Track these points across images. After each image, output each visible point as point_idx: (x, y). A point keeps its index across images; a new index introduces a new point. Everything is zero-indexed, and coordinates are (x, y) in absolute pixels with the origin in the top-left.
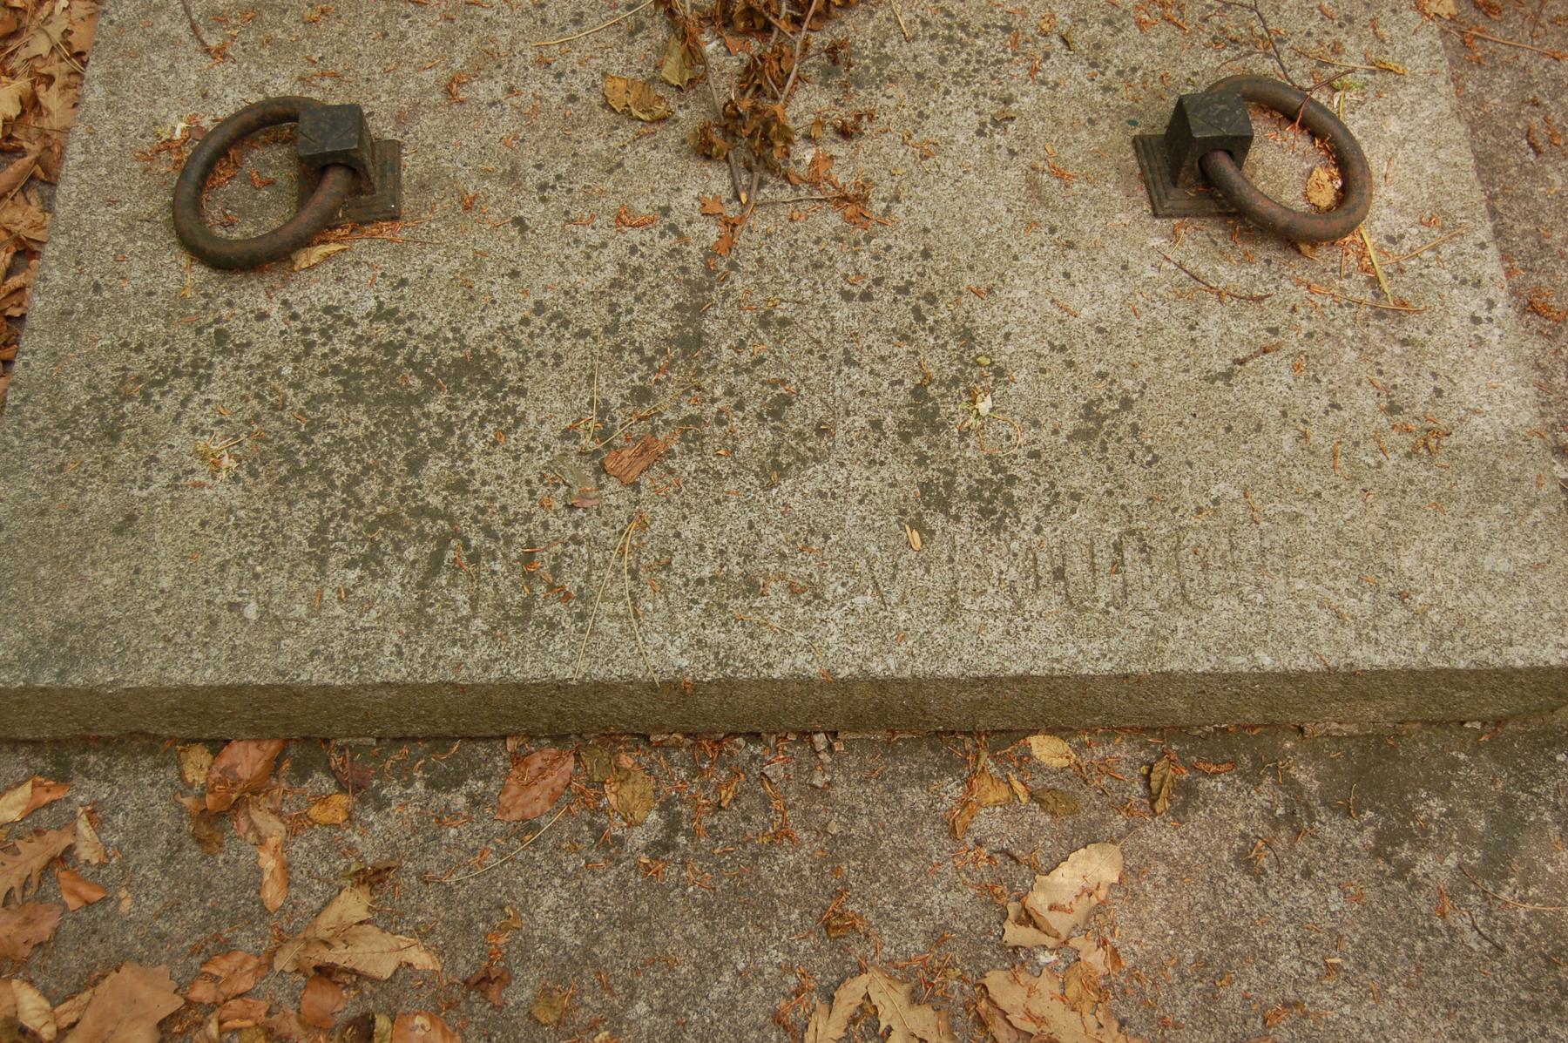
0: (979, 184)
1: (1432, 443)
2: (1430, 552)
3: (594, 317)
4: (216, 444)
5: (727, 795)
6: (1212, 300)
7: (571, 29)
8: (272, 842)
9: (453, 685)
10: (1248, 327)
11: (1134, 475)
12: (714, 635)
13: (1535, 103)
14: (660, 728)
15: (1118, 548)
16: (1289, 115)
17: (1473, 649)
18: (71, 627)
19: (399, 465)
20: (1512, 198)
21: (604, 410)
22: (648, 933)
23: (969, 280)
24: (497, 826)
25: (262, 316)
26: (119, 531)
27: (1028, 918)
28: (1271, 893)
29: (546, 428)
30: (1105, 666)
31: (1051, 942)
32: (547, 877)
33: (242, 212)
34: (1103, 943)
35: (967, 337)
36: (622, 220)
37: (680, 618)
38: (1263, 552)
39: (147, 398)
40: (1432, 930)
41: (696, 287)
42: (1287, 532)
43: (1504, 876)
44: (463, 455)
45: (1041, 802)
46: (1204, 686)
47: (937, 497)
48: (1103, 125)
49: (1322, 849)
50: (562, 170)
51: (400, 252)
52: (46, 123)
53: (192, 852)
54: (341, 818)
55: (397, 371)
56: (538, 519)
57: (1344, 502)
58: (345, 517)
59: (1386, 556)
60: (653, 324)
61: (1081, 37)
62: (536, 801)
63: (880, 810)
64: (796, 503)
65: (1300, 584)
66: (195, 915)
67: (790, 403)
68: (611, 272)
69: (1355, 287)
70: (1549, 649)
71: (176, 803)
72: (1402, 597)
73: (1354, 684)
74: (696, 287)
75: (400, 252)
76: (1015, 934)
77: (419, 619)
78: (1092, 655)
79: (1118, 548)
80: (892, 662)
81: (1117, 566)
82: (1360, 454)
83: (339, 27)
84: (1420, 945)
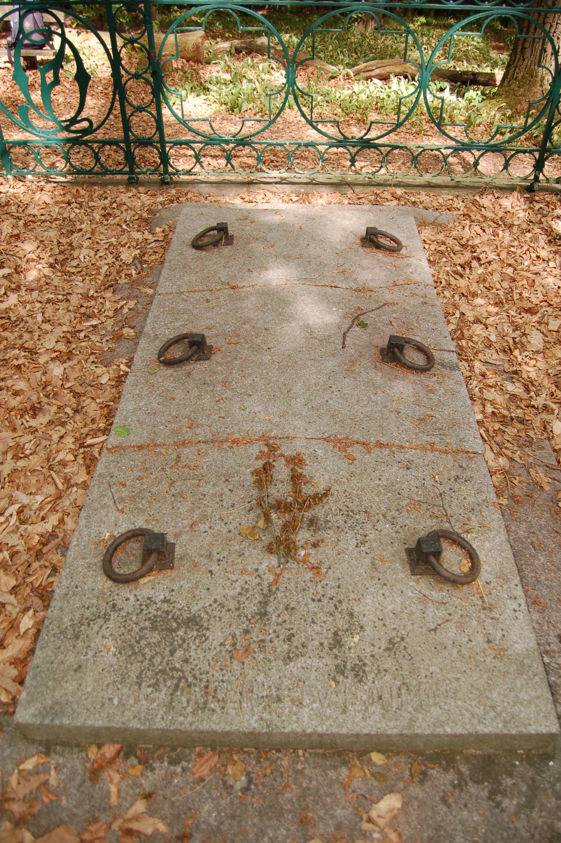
0: (356, 563)
1: (502, 653)
2: (502, 692)
3: (232, 605)
4: (110, 643)
5: (268, 771)
6: (430, 604)
7: (231, 509)
8: (116, 781)
9: (180, 730)
10: (441, 613)
11: (405, 663)
12: (266, 716)
13: (534, 533)
14: (247, 746)
15: (399, 689)
16: (454, 542)
17: (517, 727)
18: (57, 703)
19: (167, 652)
20: (528, 565)
21: (234, 637)
22: (239, 822)
23: (352, 596)
24: (191, 779)
25: (128, 599)
26: (76, 671)
27: (370, 820)
28: (454, 813)
29: (215, 642)
30: (395, 731)
31: (378, 829)
32: (207, 799)
33: (125, 564)
34: (395, 830)
35: (351, 615)
36: (244, 572)
37: (255, 710)
38: (447, 691)
39: (89, 625)
40: (509, 828)
41: (265, 596)
42: (455, 684)
43: (533, 808)
44: (188, 650)
45: (375, 777)
46: (429, 739)
47: (340, 670)
48: (396, 544)
49: (470, 796)
50: (225, 555)
51: (173, 580)
52: (65, 527)
53: (88, 784)
54: (139, 773)
55: (169, 620)
56: (211, 673)
57: (473, 674)
58: (149, 669)
59: (488, 693)
60: (251, 608)
61: (389, 514)
62: (204, 771)
63: (320, 778)
64: (295, 671)
65: (459, 703)
66: (87, 807)
67: (294, 636)
68: (239, 590)
69: (476, 599)
70: (543, 727)
71: (84, 765)
72: (493, 708)
73: (480, 739)
74: (265, 596)
75: (173, 580)
76: (366, 826)
77: (170, 706)
78: (391, 727)
79: (399, 689)
80: (325, 728)
81: (399, 696)
82: (478, 657)
83: (159, 505)
84: (505, 834)
